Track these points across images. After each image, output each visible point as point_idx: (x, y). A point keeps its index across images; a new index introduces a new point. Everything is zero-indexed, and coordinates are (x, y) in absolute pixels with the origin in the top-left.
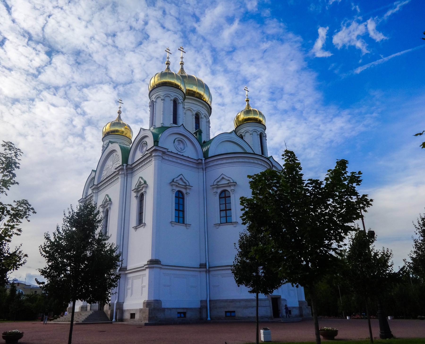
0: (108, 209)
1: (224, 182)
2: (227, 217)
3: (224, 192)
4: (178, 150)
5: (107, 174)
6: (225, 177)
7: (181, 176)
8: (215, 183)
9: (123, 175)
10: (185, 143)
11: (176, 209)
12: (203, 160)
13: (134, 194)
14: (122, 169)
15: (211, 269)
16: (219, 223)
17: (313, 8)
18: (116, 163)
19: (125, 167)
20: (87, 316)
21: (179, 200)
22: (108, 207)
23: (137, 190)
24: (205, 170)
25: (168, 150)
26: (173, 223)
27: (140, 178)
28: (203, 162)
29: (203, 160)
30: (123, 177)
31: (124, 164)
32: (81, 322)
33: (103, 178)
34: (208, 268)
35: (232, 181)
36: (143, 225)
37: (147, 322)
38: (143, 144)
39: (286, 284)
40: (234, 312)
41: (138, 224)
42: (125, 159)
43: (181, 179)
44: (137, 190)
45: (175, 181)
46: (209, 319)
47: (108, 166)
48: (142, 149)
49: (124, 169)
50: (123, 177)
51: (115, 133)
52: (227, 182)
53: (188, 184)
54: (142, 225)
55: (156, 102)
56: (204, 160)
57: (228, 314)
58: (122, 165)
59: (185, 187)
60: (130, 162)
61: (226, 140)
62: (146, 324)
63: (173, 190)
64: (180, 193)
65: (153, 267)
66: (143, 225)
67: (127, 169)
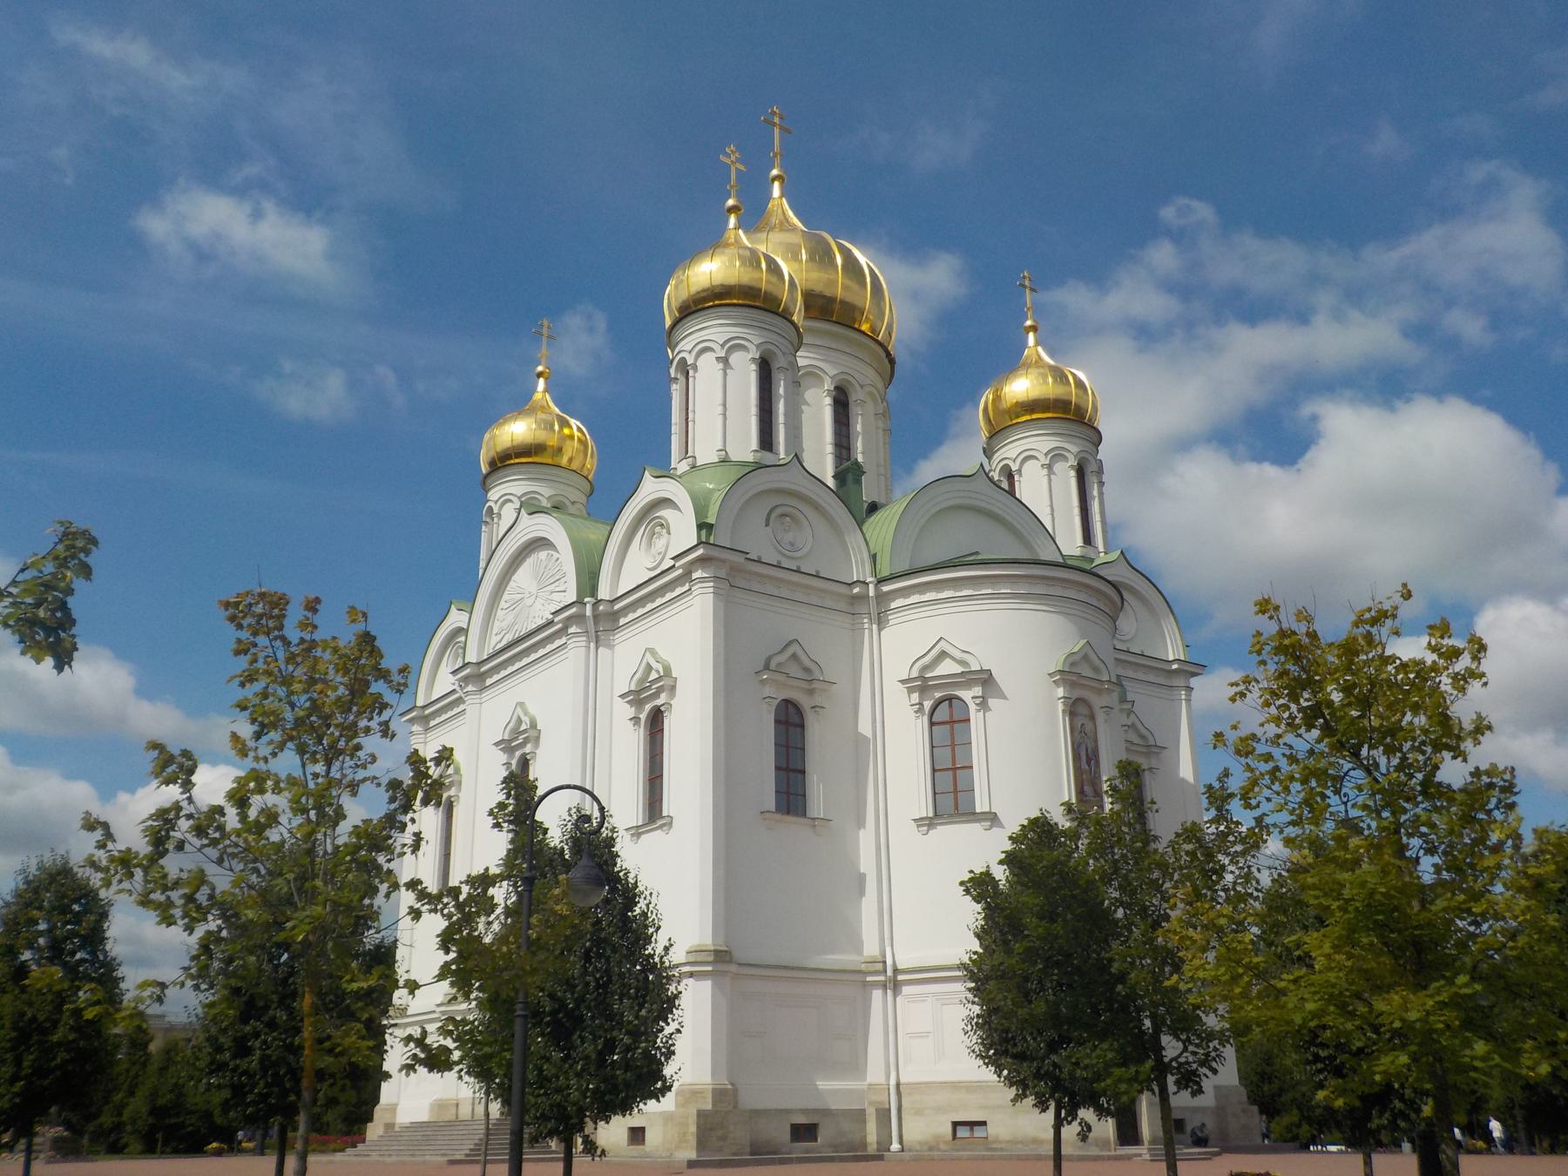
0: (528, 757)
1: (947, 668)
2: (959, 794)
3: (947, 702)
4: (783, 551)
5: (513, 624)
6: (950, 650)
7: (794, 648)
8: (915, 674)
9: (584, 639)
10: (800, 515)
11: (800, 776)
12: (871, 587)
13: (625, 711)
14: (579, 618)
15: (900, 978)
16: (931, 814)
17: (1501, 894)
18: (552, 587)
19: (589, 611)
20: (477, 1137)
21: (787, 732)
22: (528, 749)
23: (636, 697)
24: (879, 618)
25: (748, 556)
26: (767, 815)
27: (648, 654)
28: (872, 593)
29: (871, 587)
30: (584, 644)
31: (586, 600)
32: (463, 1158)
33: (499, 637)
34: (890, 973)
35: (975, 667)
36: (664, 825)
37: (693, 1155)
38: (655, 526)
39: (471, 706)
40: (984, 1123)
41: (644, 820)
42: (588, 580)
43: (794, 656)
44: (636, 697)
45: (773, 665)
46: (895, 1146)
47: (522, 596)
48: (650, 544)
49: (585, 616)
50: (584, 644)
51: (512, 462)
52: (959, 669)
53: (817, 675)
54: (659, 823)
55: (695, 367)
56: (876, 585)
57: (963, 1132)
58: (579, 602)
59: (807, 687)
60: (604, 592)
61: (951, 503)
62: (692, 1164)
63: (767, 700)
64: (790, 706)
65: (724, 973)
66: (664, 825)
67: (596, 617)
